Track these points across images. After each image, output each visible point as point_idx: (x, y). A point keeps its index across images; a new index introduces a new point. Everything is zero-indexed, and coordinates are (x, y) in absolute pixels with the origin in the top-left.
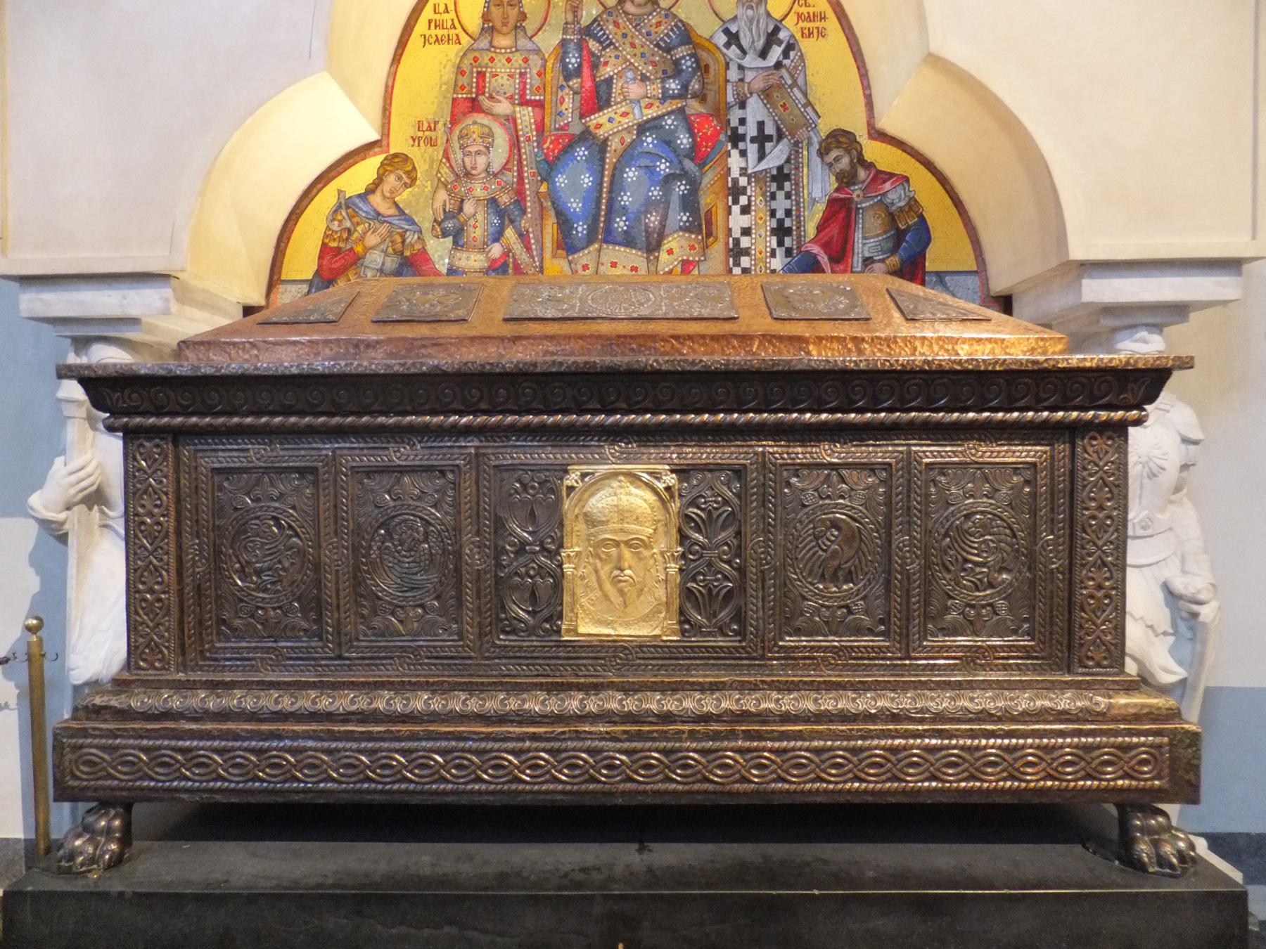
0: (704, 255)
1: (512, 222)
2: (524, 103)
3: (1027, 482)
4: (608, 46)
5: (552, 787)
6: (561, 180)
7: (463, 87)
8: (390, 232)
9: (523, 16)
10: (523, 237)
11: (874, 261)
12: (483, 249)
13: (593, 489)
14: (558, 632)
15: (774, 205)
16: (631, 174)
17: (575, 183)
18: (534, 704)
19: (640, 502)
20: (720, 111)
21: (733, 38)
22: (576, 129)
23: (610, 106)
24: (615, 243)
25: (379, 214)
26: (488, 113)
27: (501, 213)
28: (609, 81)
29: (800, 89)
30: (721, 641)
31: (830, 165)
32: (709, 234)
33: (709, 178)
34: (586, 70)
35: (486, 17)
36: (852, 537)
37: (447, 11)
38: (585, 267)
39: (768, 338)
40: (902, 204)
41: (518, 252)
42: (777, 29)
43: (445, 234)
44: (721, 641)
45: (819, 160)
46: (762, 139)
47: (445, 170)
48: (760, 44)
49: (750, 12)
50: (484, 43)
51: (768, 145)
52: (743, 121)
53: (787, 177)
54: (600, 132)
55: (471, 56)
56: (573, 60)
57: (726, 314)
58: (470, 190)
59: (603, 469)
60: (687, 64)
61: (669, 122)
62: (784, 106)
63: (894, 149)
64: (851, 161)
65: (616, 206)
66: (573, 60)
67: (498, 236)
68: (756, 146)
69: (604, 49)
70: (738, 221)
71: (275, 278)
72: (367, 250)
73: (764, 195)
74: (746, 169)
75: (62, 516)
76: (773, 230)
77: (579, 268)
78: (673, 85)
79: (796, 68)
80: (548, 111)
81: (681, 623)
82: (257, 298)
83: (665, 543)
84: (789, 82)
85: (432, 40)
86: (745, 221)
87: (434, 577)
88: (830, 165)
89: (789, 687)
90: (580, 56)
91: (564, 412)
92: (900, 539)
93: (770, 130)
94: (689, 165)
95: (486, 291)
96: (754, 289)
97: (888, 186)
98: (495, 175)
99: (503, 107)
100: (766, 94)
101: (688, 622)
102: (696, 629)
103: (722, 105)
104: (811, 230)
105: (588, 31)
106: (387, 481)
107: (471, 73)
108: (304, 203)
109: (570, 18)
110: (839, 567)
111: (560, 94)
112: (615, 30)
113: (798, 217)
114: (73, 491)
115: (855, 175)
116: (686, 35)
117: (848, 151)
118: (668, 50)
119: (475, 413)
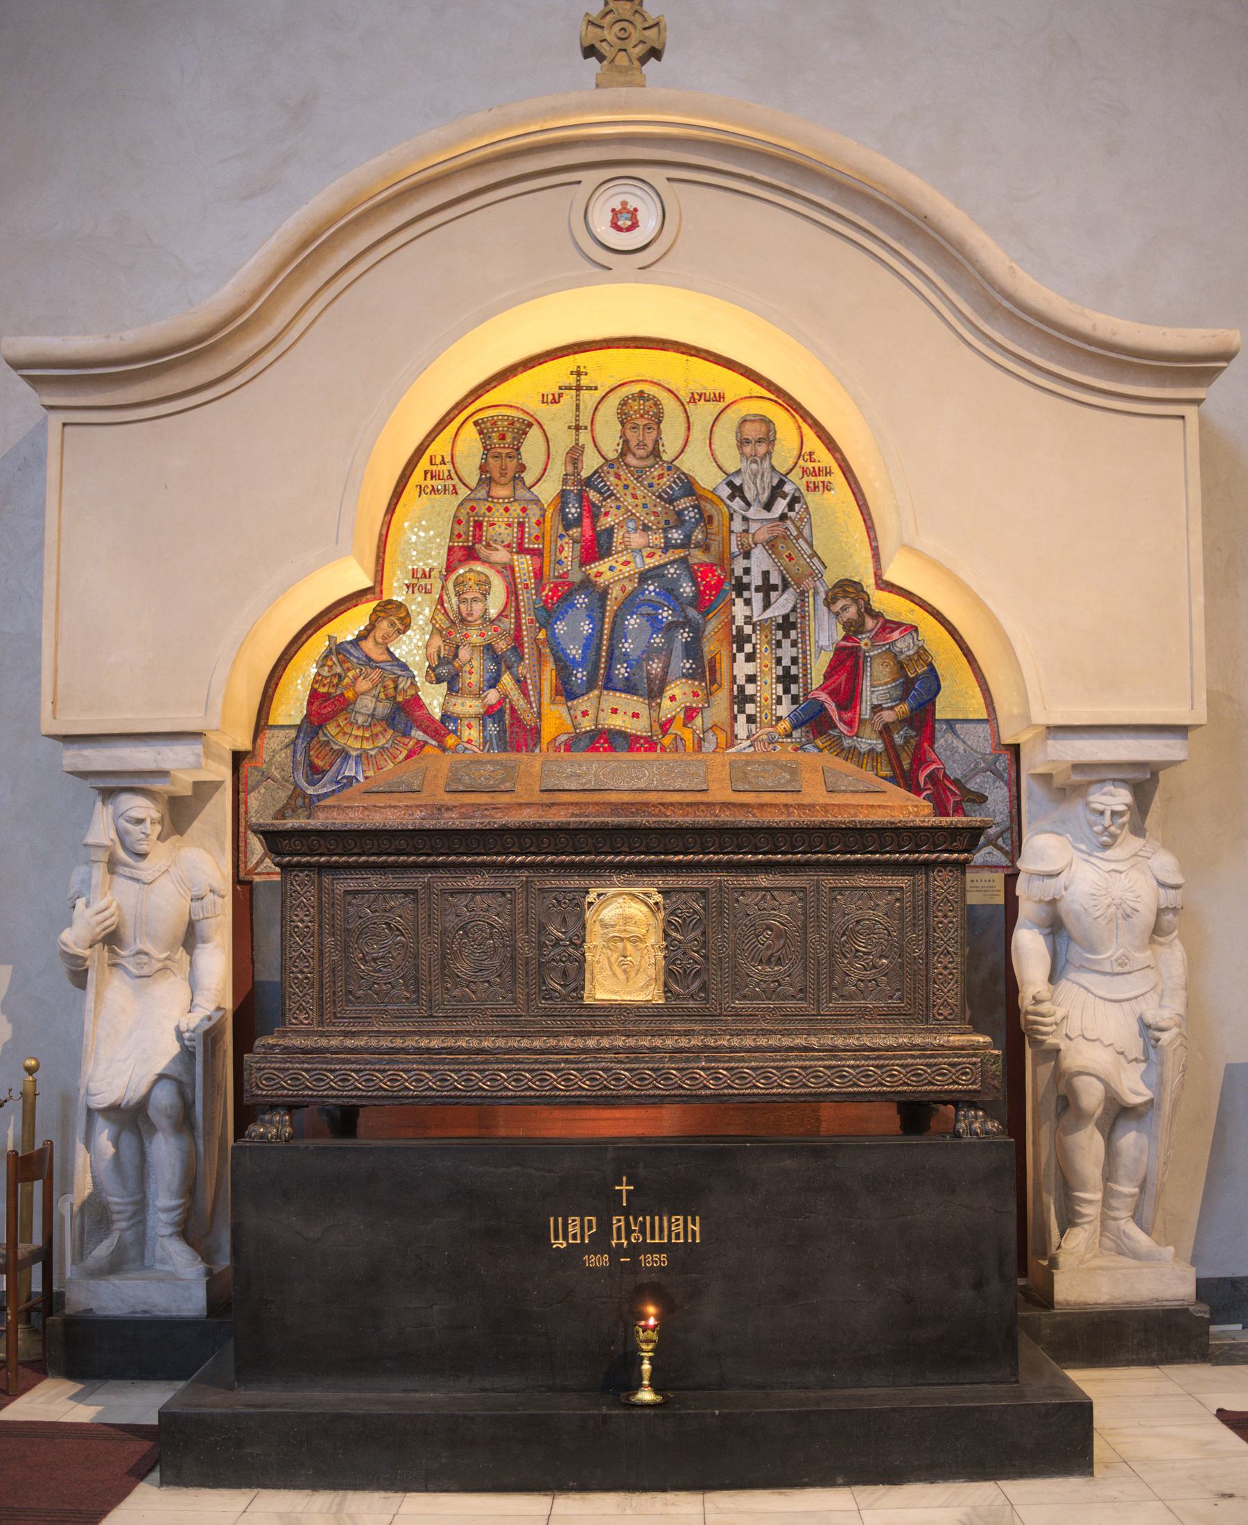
0: (708, 702)
1: (509, 668)
2: (522, 550)
3: (897, 900)
4: (609, 497)
5: (578, 1093)
6: (560, 627)
7: (459, 536)
8: (382, 679)
9: (523, 468)
10: (521, 683)
11: (883, 709)
12: (479, 695)
13: (604, 905)
14: (582, 998)
15: (780, 652)
16: (633, 622)
17: (574, 630)
18: (566, 1043)
19: (637, 912)
20: (725, 560)
21: (737, 491)
22: (575, 577)
23: (610, 555)
24: (616, 690)
25: (370, 660)
26: (485, 562)
27: (497, 658)
28: (610, 531)
29: (806, 541)
30: (691, 1004)
31: (837, 614)
32: (713, 681)
33: (713, 626)
34: (586, 521)
35: (483, 469)
36: (779, 935)
37: (443, 462)
38: (585, 714)
39: (726, 805)
40: (911, 652)
41: (515, 698)
42: (782, 483)
43: (439, 681)
44: (691, 1004)
45: (825, 609)
46: (767, 588)
47: (440, 617)
48: (765, 497)
49: (754, 466)
50: (481, 494)
51: (773, 595)
52: (747, 571)
53: (793, 626)
54: (600, 580)
55: (468, 506)
56: (573, 510)
57: (699, 788)
58: (466, 636)
59: (613, 890)
60: (690, 515)
61: (672, 571)
62: (790, 557)
63: (903, 600)
64: (859, 610)
65: (617, 652)
66: (573, 510)
67: (494, 682)
68: (760, 595)
69: (605, 500)
70: (742, 669)
71: (262, 723)
72: (357, 695)
73: (769, 643)
74: (751, 618)
75: (87, 953)
76: (778, 678)
77: (579, 714)
78: (676, 535)
79: (801, 519)
80: (546, 560)
81: (665, 992)
82: (244, 743)
83: (654, 938)
84: (795, 533)
85: (428, 490)
86: (750, 668)
87: (496, 962)
88: (837, 614)
89: (739, 1033)
90: (580, 507)
91: (587, 853)
92: (813, 936)
93: (775, 579)
94: (692, 613)
95: (523, 767)
96: (723, 766)
97: (896, 635)
98: (492, 622)
99: (501, 556)
100: (771, 545)
101: (670, 991)
102: (677, 996)
103: (727, 555)
104: (817, 679)
105: (588, 482)
106: (463, 900)
107: (468, 522)
108: (293, 649)
109: (570, 469)
110: (772, 955)
111: (559, 543)
112: (617, 481)
113: (805, 664)
114: (98, 929)
115: (863, 624)
116: (688, 486)
117: (856, 601)
118: (671, 501)
119: (527, 854)
